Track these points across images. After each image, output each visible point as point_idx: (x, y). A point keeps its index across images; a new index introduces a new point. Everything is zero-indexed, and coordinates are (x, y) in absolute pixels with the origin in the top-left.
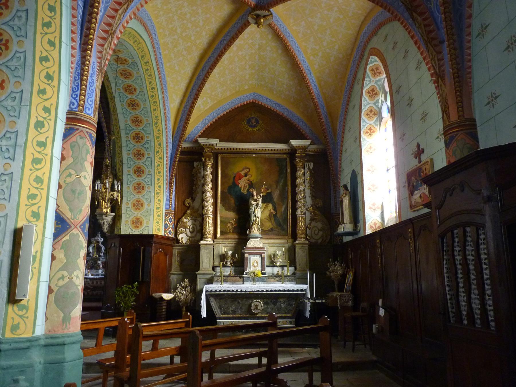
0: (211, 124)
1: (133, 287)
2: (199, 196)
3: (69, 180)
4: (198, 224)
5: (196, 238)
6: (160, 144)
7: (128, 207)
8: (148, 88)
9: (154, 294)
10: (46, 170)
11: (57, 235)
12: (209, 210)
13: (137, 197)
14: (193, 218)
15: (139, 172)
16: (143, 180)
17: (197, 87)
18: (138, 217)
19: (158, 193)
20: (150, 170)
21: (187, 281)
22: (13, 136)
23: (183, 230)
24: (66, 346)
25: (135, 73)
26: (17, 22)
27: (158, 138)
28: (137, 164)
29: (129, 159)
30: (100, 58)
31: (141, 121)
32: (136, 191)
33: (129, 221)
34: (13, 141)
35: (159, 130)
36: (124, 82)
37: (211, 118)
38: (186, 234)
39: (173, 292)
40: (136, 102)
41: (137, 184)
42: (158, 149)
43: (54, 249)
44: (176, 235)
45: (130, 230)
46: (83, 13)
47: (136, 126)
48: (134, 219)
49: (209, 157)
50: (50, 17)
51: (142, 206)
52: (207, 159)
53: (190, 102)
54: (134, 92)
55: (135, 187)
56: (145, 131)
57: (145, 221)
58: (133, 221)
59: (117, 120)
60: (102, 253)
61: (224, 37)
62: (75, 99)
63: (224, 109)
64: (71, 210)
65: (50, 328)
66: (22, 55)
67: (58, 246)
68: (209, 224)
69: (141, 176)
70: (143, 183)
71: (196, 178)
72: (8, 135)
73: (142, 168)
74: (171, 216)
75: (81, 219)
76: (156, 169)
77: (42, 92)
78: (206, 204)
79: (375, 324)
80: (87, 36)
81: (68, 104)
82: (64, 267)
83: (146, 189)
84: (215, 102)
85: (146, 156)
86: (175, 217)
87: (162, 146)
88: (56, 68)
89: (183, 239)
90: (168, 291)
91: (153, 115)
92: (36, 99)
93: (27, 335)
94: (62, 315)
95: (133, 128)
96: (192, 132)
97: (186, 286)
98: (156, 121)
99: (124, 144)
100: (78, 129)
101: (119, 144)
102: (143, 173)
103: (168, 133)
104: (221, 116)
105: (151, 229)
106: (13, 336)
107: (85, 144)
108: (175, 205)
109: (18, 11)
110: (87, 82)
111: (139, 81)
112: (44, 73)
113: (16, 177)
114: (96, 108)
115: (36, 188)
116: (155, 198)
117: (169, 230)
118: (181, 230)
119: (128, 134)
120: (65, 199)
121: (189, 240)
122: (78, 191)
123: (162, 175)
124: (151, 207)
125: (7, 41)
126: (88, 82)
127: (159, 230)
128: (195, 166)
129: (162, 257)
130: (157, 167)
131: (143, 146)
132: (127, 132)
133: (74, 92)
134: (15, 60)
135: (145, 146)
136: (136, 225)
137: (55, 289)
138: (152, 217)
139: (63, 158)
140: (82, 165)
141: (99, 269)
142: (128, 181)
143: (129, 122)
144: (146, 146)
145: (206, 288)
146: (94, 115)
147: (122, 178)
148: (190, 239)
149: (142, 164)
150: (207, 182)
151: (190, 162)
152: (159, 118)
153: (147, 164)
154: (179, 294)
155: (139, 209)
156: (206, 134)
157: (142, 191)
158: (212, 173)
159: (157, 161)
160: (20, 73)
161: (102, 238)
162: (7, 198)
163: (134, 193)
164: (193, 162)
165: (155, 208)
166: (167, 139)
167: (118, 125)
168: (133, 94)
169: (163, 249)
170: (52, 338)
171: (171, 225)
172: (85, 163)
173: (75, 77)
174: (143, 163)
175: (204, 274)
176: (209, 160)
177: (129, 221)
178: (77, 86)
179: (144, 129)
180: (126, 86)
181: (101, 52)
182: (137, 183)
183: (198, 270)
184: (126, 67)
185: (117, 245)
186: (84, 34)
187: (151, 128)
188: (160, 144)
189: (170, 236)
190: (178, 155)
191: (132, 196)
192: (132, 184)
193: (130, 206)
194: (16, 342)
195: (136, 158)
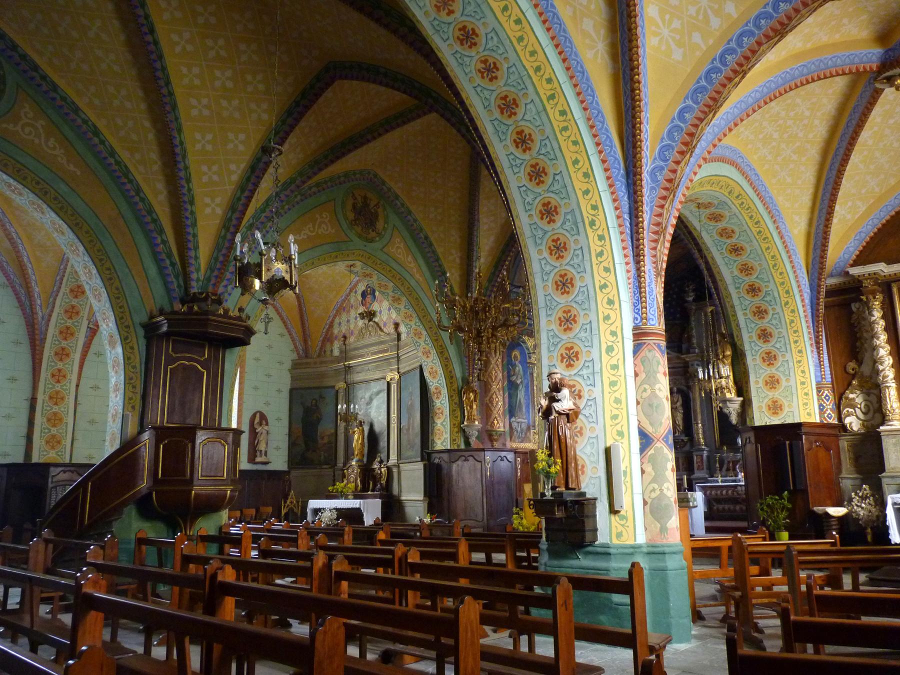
0: (871, 238)
1: (782, 498)
2: (867, 355)
3: (645, 395)
4: (874, 398)
5: (874, 422)
6: (787, 292)
8: (750, 225)
9: (815, 509)
10: (623, 390)
11: (642, 450)
12: (888, 376)
13: (768, 372)
14: (864, 391)
15: (765, 335)
16: (773, 346)
17: (828, 195)
19: (799, 362)
20: (780, 330)
21: (867, 489)
22: (590, 364)
23: (851, 410)
24: (667, 555)
25: (727, 214)
26: (576, 261)
27: (783, 283)
29: (748, 321)
30: (654, 263)
31: (752, 268)
34: (591, 370)
35: (781, 274)
36: (715, 226)
37: (869, 228)
38: (857, 416)
39: (847, 505)
40: (739, 245)
42: (786, 300)
43: (642, 463)
44: (840, 419)
45: (766, 418)
46: (631, 224)
47: (747, 275)
48: (770, 403)
49: (874, 293)
50: (601, 246)
52: (871, 297)
53: (823, 219)
54: (733, 235)
55: (763, 358)
56: (762, 279)
58: (769, 406)
59: (719, 273)
61: (851, 115)
62: (637, 313)
63: (890, 208)
64: (651, 424)
65: (650, 538)
66: (585, 289)
67: (646, 460)
68: (892, 399)
69: (769, 341)
70: (774, 351)
71: (860, 329)
72: (586, 365)
73: (769, 330)
74: (826, 392)
75: (662, 432)
76: (789, 327)
77: (607, 318)
78: (881, 368)
80: (637, 247)
81: (632, 320)
82: (654, 480)
83: (780, 359)
84: (872, 201)
85: (771, 312)
86: (834, 392)
87: (791, 294)
88: (615, 292)
89: (853, 425)
90: (839, 504)
91: (767, 257)
92: (603, 326)
93: (630, 542)
94: (659, 526)
96: (840, 258)
97: (866, 496)
98: (773, 263)
99: (736, 302)
100: (645, 343)
101: (731, 303)
102: (771, 336)
103: (798, 271)
104: (887, 221)
105: (796, 414)
106: (618, 542)
107: (655, 357)
108: (831, 374)
109: (575, 250)
110: (645, 293)
111: (736, 220)
112: (606, 300)
113: (599, 401)
114: (660, 315)
115: (617, 409)
116: (796, 369)
117: (828, 412)
118: (848, 411)
119: (739, 288)
120: (644, 414)
121: (863, 425)
122: (655, 405)
123: (801, 334)
124: (792, 383)
125: (572, 279)
126: (647, 292)
127: (809, 414)
128: (854, 309)
129: (822, 453)
130: (790, 324)
132: (737, 285)
133: (635, 307)
134: (580, 295)
135: (765, 299)
137: (649, 501)
139: (636, 375)
140: (655, 378)
143: (736, 273)
144: (768, 299)
145: (892, 498)
146: (660, 323)
148: (864, 423)
150: (876, 333)
151: (845, 306)
152: (778, 256)
154: (855, 507)
155: (775, 388)
156: (863, 258)
157: (775, 362)
158: (883, 317)
159: (788, 317)
160: (586, 306)
162: (595, 421)
163: (764, 366)
164: (850, 305)
165: (799, 384)
166: (797, 282)
167: (723, 280)
168: (731, 237)
169: (822, 442)
170: (653, 546)
171: (829, 406)
172: (658, 375)
173: (634, 292)
174: (768, 323)
175: (893, 477)
176: (874, 298)
178: (638, 300)
180: (720, 231)
181: (655, 256)
183: (884, 471)
184: (713, 210)
185: (753, 440)
186: (635, 246)
187: (769, 273)
188: (787, 292)
189: (831, 421)
190: (821, 300)
191: (761, 371)
194: (622, 548)
195: (756, 318)
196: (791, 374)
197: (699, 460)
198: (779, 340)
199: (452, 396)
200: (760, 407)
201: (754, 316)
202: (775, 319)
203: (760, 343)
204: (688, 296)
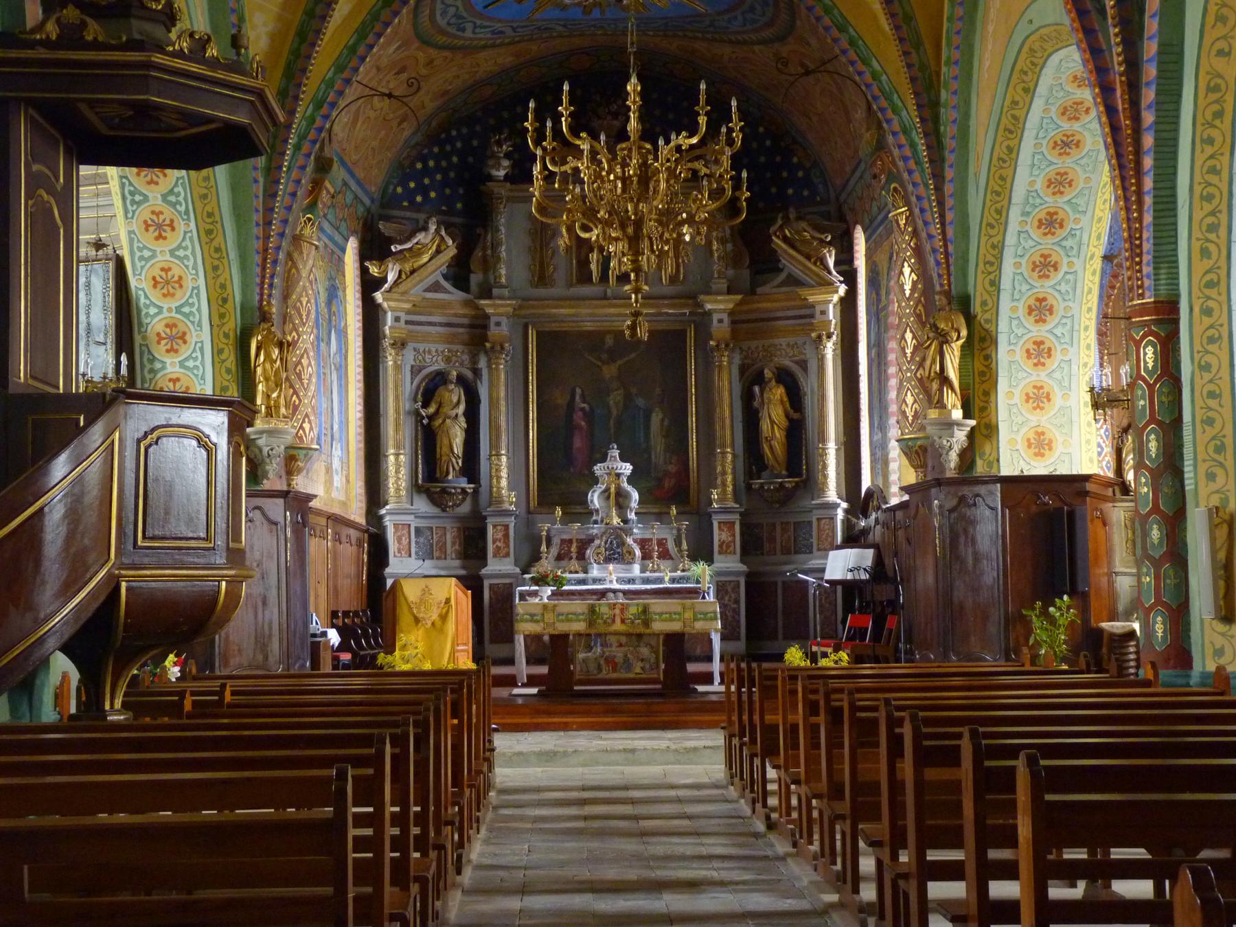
7: (1012, 402)
13: (1034, 378)
16: (1050, 331)
18: (1040, 430)
20: (1071, 304)
28: (1036, 290)
32: (1031, 362)
33: (1019, 440)
41: (1035, 343)
45: (1022, 462)
48: (1032, 435)
51: (1049, 400)
55: (1028, 351)
56: (1075, 207)
57: (1060, 439)
58: (1028, 440)
60: (631, 511)
70: (1050, 341)
73: (1051, 301)
79: (838, 872)
83: (1058, 356)
85: (1064, 268)
95: (1046, 199)
119: (1028, 214)
131: (1058, 244)
132: (1028, 209)
135: (1064, 243)
136: (1037, 450)
138: (1075, 428)
141: (631, 562)
142: (1012, 336)
143: (1040, 185)
147: (993, 328)
149: (1050, 290)
153: (1063, 291)
155: (1042, 409)
157: (1047, 361)
161: (624, 464)
163: (1028, 365)
174: (1053, 287)
177: (1019, 440)
179: (1073, 201)
182: (1034, 339)
191: (1021, 375)
192: (1021, 342)
193: (1018, 402)
196: (1073, 387)
197: (500, 535)
198: (1064, 321)
199: (220, 351)
200: (1012, 441)
201: (1033, 270)
202: (1068, 282)
203: (1029, 322)
204: (498, 167)
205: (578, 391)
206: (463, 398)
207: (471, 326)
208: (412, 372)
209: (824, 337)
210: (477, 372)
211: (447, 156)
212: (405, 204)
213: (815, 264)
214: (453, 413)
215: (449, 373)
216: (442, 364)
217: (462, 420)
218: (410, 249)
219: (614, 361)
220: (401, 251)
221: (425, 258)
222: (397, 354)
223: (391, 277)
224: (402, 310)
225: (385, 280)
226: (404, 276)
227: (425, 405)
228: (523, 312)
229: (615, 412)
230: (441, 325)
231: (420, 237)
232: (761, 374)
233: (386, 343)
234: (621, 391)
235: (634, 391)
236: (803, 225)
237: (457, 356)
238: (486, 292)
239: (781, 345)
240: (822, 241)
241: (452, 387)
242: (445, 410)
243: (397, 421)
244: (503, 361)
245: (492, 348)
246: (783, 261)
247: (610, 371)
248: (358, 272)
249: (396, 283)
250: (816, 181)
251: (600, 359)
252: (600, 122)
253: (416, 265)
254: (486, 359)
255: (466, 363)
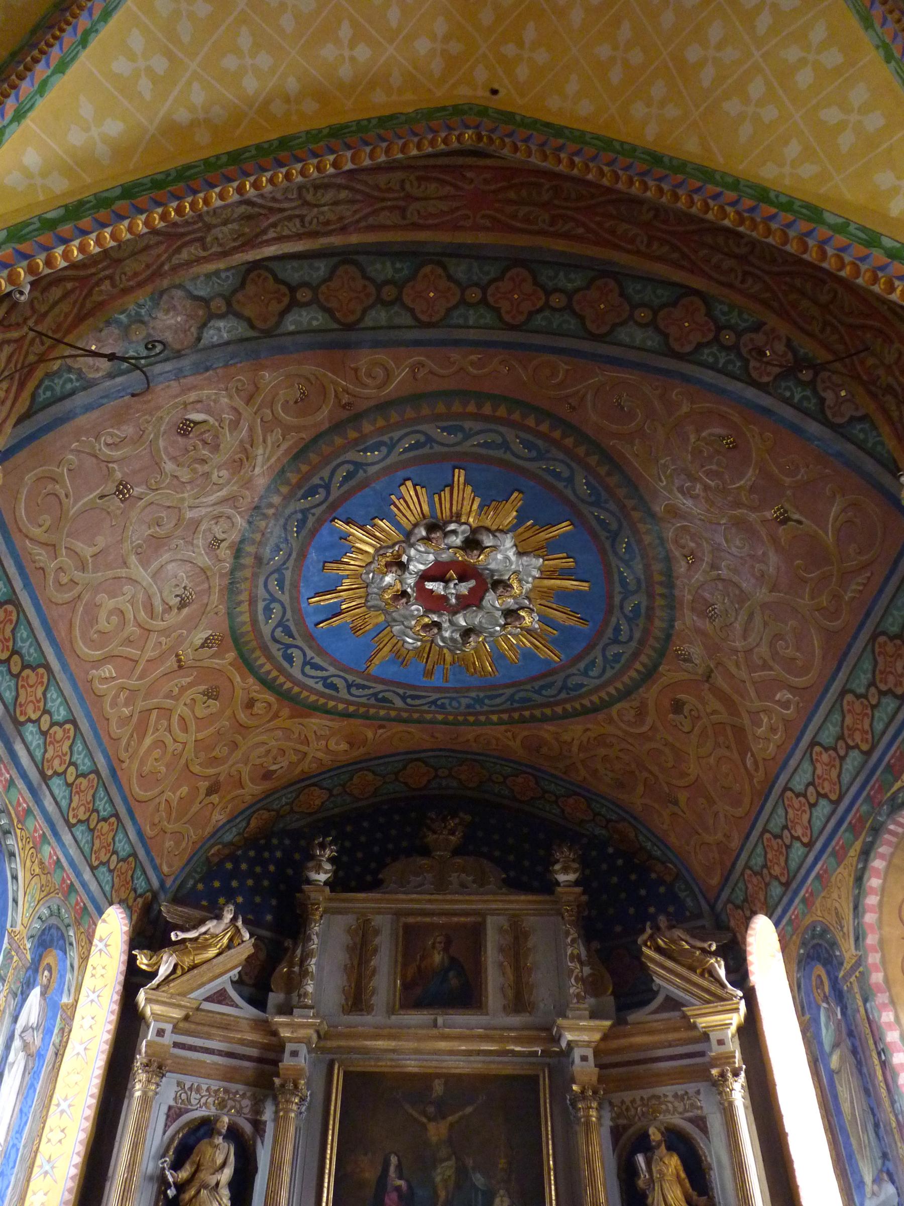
204: (319, 869)
205: (394, 1160)
206: (232, 1158)
207: (259, 1060)
208: (168, 1116)
209: (729, 1075)
210: (258, 1126)
211: (264, 863)
212: (204, 903)
213: (702, 975)
214: (213, 1180)
215: (217, 1119)
216: (213, 1109)
217: (225, 1193)
218: (196, 939)
219: (444, 1118)
220: (184, 941)
221: (212, 952)
222: (149, 1081)
223: (164, 970)
224: (167, 1019)
225: (154, 974)
226: (179, 972)
227: (176, 1166)
228: (329, 1044)
229: (442, 1194)
230: (220, 1053)
231: (210, 925)
232: (645, 1136)
233: (140, 1059)
234: (452, 1163)
235: (470, 1162)
236: (678, 933)
237: (234, 1100)
238: (286, 1009)
239: (666, 1096)
240: (704, 951)
241: (219, 1140)
242: (203, 1175)
243: (127, 1183)
244: (295, 1107)
245: (283, 1086)
246: (657, 981)
247: (437, 1131)
248: (123, 968)
249: (167, 980)
250: (682, 895)
251: (424, 1113)
252: (435, 836)
253: (198, 959)
254: (273, 1108)
255: (246, 1110)
